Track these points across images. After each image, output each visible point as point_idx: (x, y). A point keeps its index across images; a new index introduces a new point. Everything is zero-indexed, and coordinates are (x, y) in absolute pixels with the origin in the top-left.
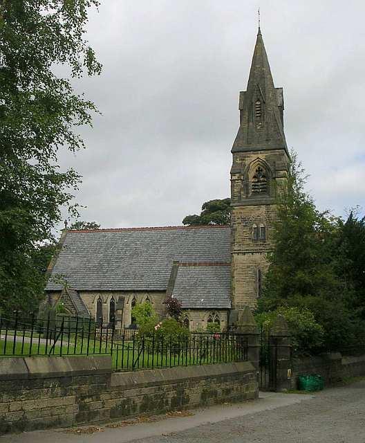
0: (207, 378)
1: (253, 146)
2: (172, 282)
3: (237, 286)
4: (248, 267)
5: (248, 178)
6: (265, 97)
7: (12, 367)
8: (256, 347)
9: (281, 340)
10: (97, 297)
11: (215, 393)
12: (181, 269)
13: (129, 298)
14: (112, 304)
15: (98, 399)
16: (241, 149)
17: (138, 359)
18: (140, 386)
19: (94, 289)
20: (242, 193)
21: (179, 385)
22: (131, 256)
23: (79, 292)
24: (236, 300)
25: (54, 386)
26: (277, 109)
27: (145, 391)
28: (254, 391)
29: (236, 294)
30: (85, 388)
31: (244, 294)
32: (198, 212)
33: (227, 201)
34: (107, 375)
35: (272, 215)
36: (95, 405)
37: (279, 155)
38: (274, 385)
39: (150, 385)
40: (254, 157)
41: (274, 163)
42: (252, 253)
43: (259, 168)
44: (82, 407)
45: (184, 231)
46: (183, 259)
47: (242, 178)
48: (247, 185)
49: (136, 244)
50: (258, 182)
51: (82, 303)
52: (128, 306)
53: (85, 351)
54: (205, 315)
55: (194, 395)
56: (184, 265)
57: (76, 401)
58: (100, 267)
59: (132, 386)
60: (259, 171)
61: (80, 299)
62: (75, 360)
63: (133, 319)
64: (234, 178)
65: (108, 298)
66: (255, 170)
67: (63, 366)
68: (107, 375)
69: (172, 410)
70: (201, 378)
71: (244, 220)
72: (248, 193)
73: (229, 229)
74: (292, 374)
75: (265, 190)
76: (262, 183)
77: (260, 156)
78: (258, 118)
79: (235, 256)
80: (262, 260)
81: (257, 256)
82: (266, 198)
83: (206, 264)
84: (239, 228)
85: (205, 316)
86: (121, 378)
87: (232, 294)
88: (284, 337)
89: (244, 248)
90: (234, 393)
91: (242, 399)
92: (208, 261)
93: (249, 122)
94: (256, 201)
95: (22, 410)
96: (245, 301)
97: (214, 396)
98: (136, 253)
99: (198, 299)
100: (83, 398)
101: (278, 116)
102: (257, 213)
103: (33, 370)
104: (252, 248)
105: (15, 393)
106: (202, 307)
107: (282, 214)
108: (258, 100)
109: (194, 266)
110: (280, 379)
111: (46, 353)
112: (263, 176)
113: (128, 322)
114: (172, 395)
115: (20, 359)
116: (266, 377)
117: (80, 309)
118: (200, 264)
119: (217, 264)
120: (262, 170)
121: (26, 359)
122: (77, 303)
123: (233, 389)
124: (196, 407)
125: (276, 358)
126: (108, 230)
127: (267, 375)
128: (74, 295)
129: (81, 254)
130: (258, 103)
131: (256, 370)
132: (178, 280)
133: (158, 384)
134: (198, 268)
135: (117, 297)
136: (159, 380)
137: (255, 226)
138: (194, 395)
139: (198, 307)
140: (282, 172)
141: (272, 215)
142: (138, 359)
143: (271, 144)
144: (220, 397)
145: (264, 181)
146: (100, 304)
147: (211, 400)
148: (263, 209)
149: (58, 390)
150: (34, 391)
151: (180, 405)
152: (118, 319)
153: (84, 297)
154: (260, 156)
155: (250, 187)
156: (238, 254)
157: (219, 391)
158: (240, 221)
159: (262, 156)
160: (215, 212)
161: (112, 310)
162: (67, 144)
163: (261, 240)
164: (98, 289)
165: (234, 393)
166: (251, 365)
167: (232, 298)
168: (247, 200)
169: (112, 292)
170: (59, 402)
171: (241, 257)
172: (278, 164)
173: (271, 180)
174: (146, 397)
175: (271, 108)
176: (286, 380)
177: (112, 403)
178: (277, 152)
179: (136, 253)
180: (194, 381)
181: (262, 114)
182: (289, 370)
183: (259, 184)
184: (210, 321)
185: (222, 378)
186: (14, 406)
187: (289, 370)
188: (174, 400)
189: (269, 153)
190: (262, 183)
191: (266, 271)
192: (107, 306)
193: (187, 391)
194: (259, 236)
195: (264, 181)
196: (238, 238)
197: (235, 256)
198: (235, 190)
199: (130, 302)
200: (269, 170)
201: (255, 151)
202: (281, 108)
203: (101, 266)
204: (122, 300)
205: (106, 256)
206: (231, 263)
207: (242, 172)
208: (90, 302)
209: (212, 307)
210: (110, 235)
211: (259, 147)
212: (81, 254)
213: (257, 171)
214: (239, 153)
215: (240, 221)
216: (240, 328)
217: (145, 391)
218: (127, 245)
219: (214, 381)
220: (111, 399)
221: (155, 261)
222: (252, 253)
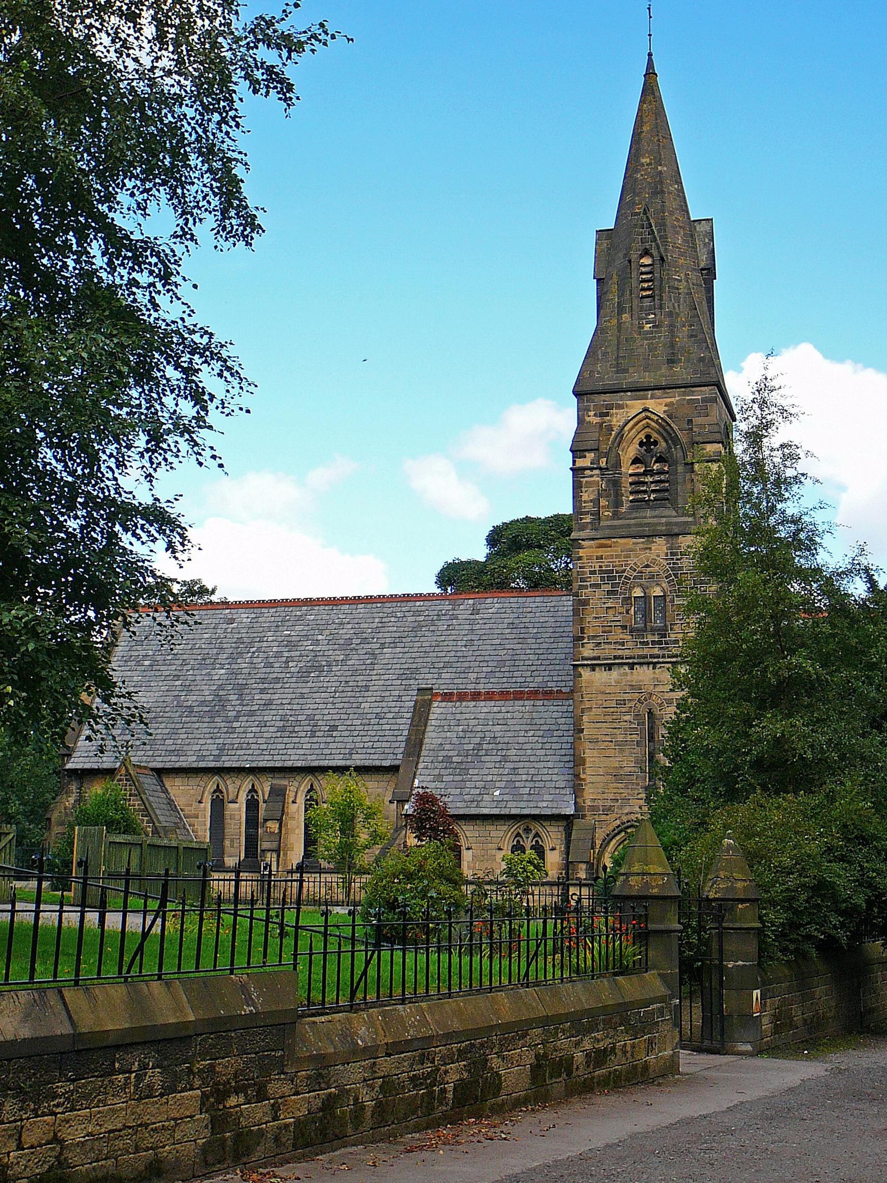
0: (545, 1022)
1: (635, 377)
2: (415, 745)
3: (590, 754)
4: (622, 703)
5: (618, 464)
6: (665, 243)
7: (26, 1017)
8: (669, 932)
9: (732, 909)
10: (211, 787)
11: (565, 1065)
12: (438, 709)
13: (297, 792)
14: (252, 805)
15: (262, 1095)
16: (599, 385)
17: (365, 973)
18: (370, 1052)
19: (202, 765)
20: (603, 502)
21: (475, 1045)
22: (303, 675)
23: (160, 773)
24: (589, 795)
25: (144, 1067)
26: (694, 276)
27: (386, 1064)
28: (668, 1052)
29: (588, 775)
30: (228, 1066)
31: (614, 784)
32: (479, 552)
33: (558, 526)
34: (282, 1026)
35: (686, 563)
36: (253, 1113)
37: (704, 400)
38: (714, 1037)
39: (392, 1049)
40: (635, 406)
41: (690, 422)
42: (631, 666)
43: (648, 437)
44: (218, 1123)
45: (446, 606)
46: (444, 682)
47: (603, 463)
48: (615, 484)
49: (317, 642)
50: (645, 474)
51: (170, 802)
52: (297, 811)
53: (223, 962)
54: (504, 835)
55: (513, 1071)
56: (447, 697)
57: (203, 1104)
58: (217, 706)
59: (355, 1053)
60: (647, 443)
61: (165, 791)
62: (203, 989)
63: (310, 841)
64: (580, 463)
65: (239, 791)
66: (637, 441)
67: (171, 1007)
68: (282, 1026)
69: (453, 1119)
70: (531, 1023)
71: (609, 575)
72: (618, 504)
73: (567, 602)
74: (763, 1006)
75: (666, 497)
76: (657, 478)
77: (651, 404)
78: (647, 303)
79: (586, 673)
80: (661, 686)
81: (643, 674)
82: (667, 516)
83: (504, 695)
84: (597, 598)
85: (503, 836)
86: (318, 1035)
87: (577, 776)
88: (742, 901)
89: (608, 651)
90: (616, 1064)
91: (638, 1078)
92: (497, 688)
93: (621, 310)
94: (641, 525)
95: (56, 1139)
96: (611, 796)
97: (564, 1076)
98: (316, 667)
99: (486, 789)
100: (222, 1094)
101: (699, 296)
102: (638, 559)
103: (87, 1023)
104: (627, 653)
105: (35, 1097)
106: (496, 811)
107: (714, 565)
108: (646, 253)
109: (473, 700)
110: (730, 1016)
111: (120, 972)
112: (660, 460)
113: (296, 854)
114: (454, 1073)
115: (50, 993)
116: (693, 1016)
117: (164, 819)
118: (490, 696)
119: (533, 694)
120: (655, 443)
121: (67, 994)
122: (156, 800)
123: (613, 1049)
124: (517, 1104)
125: (721, 961)
126: (238, 605)
127: (697, 1013)
128: (149, 782)
129: (166, 670)
130: (646, 261)
131: (672, 997)
132: (431, 738)
133: (421, 1047)
134: (484, 707)
135: (265, 787)
136: (424, 1032)
137: (638, 592)
138: (513, 1071)
139: (486, 811)
140: (710, 448)
141: (686, 563)
142: (365, 973)
143: (682, 372)
144: (581, 1072)
145: (660, 472)
146: (218, 805)
147: (557, 1085)
148: (660, 546)
149: (155, 1077)
150: (90, 1083)
151: (476, 1101)
152: (266, 845)
153: (177, 788)
154: (651, 404)
155: (626, 481)
156: (593, 667)
157: (579, 1057)
158: (596, 579)
159: (658, 406)
160: (521, 555)
161: (252, 822)
162: (827, 536)
163: (653, 630)
164: (212, 765)
165: (616, 1064)
166: (658, 982)
167: (577, 789)
168: (616, 523)
169: (253, 771)
170: (155, 1112)
171: (600, 677)
172: (702, 426)
173: (680, 469)
174: (389, 1086)
175: (682, 276)
176: (748, 1020)
177: (301, 1105)
178: (698, 395)
179: (316, 667)
180: (516, 1031)
181: (656, 290)
182: (757, 993)
183: (649, 479)
184: (518, 848)
185: (581, 1023)
186: (37, 1130)
187: (757, 993)
188: (461, 1087)
189: (675, 398)
190: (657, 478)
191: (669, 713)
192: (237, 811)
193: (495, 1062)
194: (648, 621)
195: (660, 472)
196: (592, 626)
197: (586, 673)
198: (585, 497)
199: (301, 800)
200: (676, 440)
201: (639, 390)
202: (709, 273)
203: (221, 701)
204: (278, 793)
205: (233, 673)
206: (572, 691)
207: (604, 448)
208: (191, 799)
209: (526, 812)
210: (244, 616)
211: (648, 378)
212: (166, 670)
213: (641, 444)
214: (596, 398)
215: (596, 579)
216: (626, 881)
217: (386, 1064)
218: (291, 645)
219: (563, 1031)
220: (297, 1093)
221: (367, 688)
222: (631, 666)
